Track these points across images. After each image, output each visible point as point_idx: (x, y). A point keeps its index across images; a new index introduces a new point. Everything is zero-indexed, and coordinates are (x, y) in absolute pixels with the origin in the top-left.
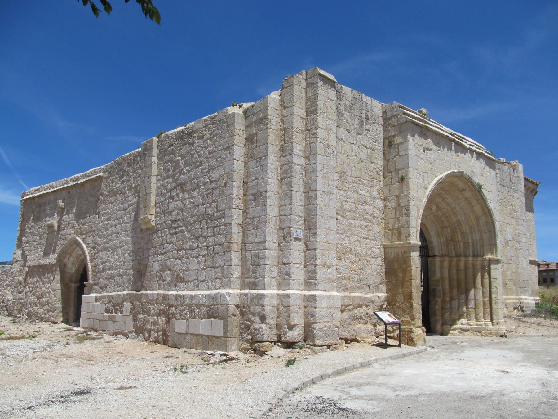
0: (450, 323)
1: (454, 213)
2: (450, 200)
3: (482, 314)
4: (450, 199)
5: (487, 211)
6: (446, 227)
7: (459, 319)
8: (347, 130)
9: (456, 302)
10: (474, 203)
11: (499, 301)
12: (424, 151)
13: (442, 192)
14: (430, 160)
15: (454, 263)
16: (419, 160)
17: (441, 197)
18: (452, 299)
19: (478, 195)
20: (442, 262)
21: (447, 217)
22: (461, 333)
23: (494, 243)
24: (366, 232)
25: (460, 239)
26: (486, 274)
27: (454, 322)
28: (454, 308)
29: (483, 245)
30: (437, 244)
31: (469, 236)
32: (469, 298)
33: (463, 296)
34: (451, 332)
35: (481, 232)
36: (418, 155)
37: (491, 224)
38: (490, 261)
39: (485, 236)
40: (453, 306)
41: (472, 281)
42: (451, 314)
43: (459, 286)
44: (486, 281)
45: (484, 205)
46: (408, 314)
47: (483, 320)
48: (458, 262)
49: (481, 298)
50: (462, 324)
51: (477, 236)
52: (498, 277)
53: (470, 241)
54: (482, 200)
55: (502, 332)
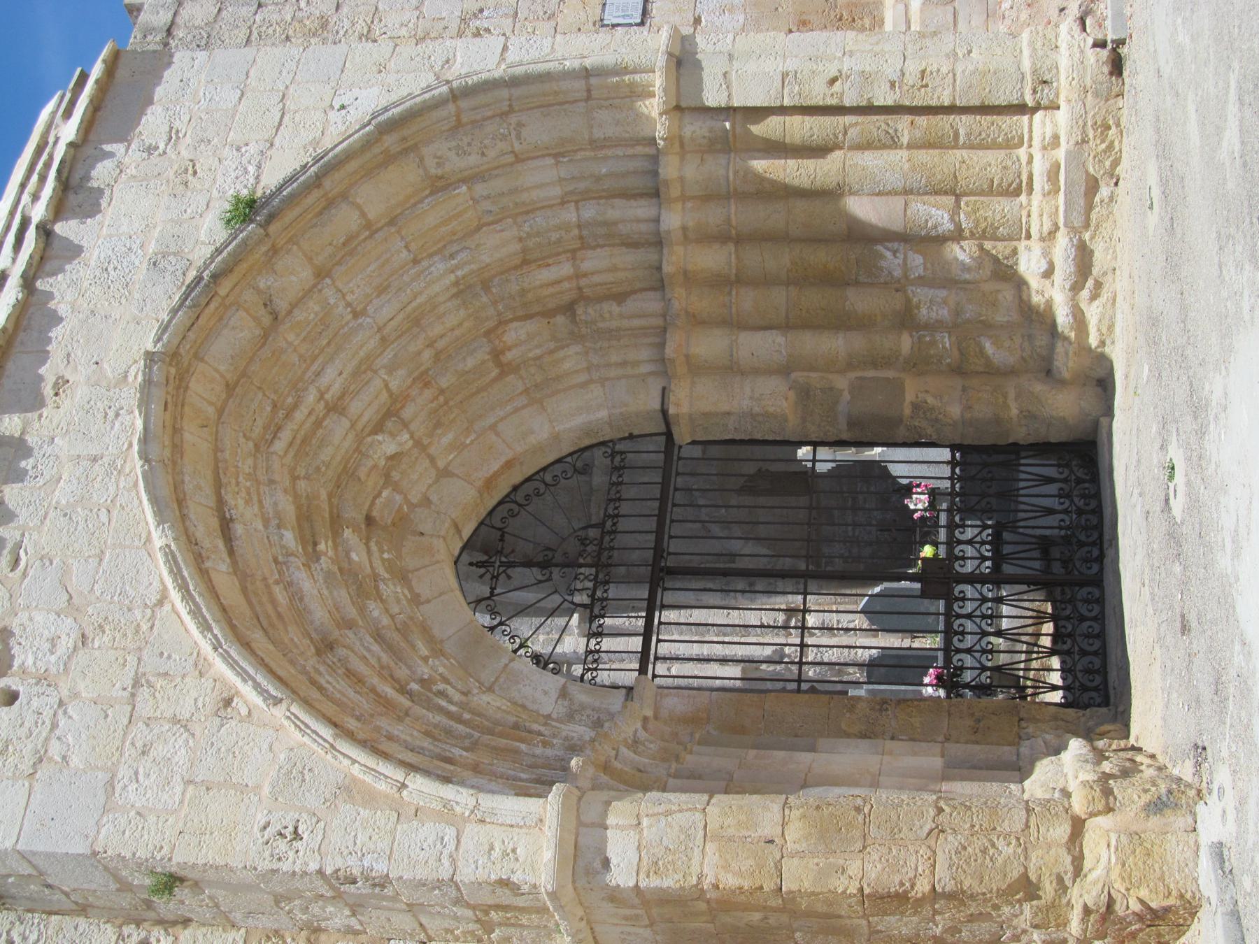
0: (1042, 340)
1: (416, 321)
2: (333, 378)
3: (992, 157)
4: (330, 373)
5: (390, 141)
6: (496, 355)
7: (1020, 284)
9: (920, 294)
10: (346, 220)
11: (913, 68)
13: (279, 446)
14: (65, 644)
15: (703, 303)
16: (55, 749)
17: (318, 424)
18: (906, 319)
19: (290, 215)
20: (697, 369)
21: (437, 357)
22: (1098, 285)
23: (580, 85)
25: (566, 269)
26: (756, 129)
27: (1037, 320)
28: (957, 313)
29: (595, 144)
30: (596, 391)
31: (539, 220)
32: (897, 225)
33: (891, 260)
34: (1093, 341)
35: (519, 159)
36: (26, 767)
37: (464, 104)
38: (684, 107)
39: (538, 131)
40: (944, 313)
41: (800, 205)
42: (986, 326)
43: (831, 280)
44: (799, 128)
45: (353, 165)
46: (996, 907)
47: (1022, 152)
48: (689, 278)
49: (898, 157)
50: (1048, 273)
51: (542, 179)
52: (773, 67)
53: (569, 215)
54: (327, 183)
55: (1096, 60)
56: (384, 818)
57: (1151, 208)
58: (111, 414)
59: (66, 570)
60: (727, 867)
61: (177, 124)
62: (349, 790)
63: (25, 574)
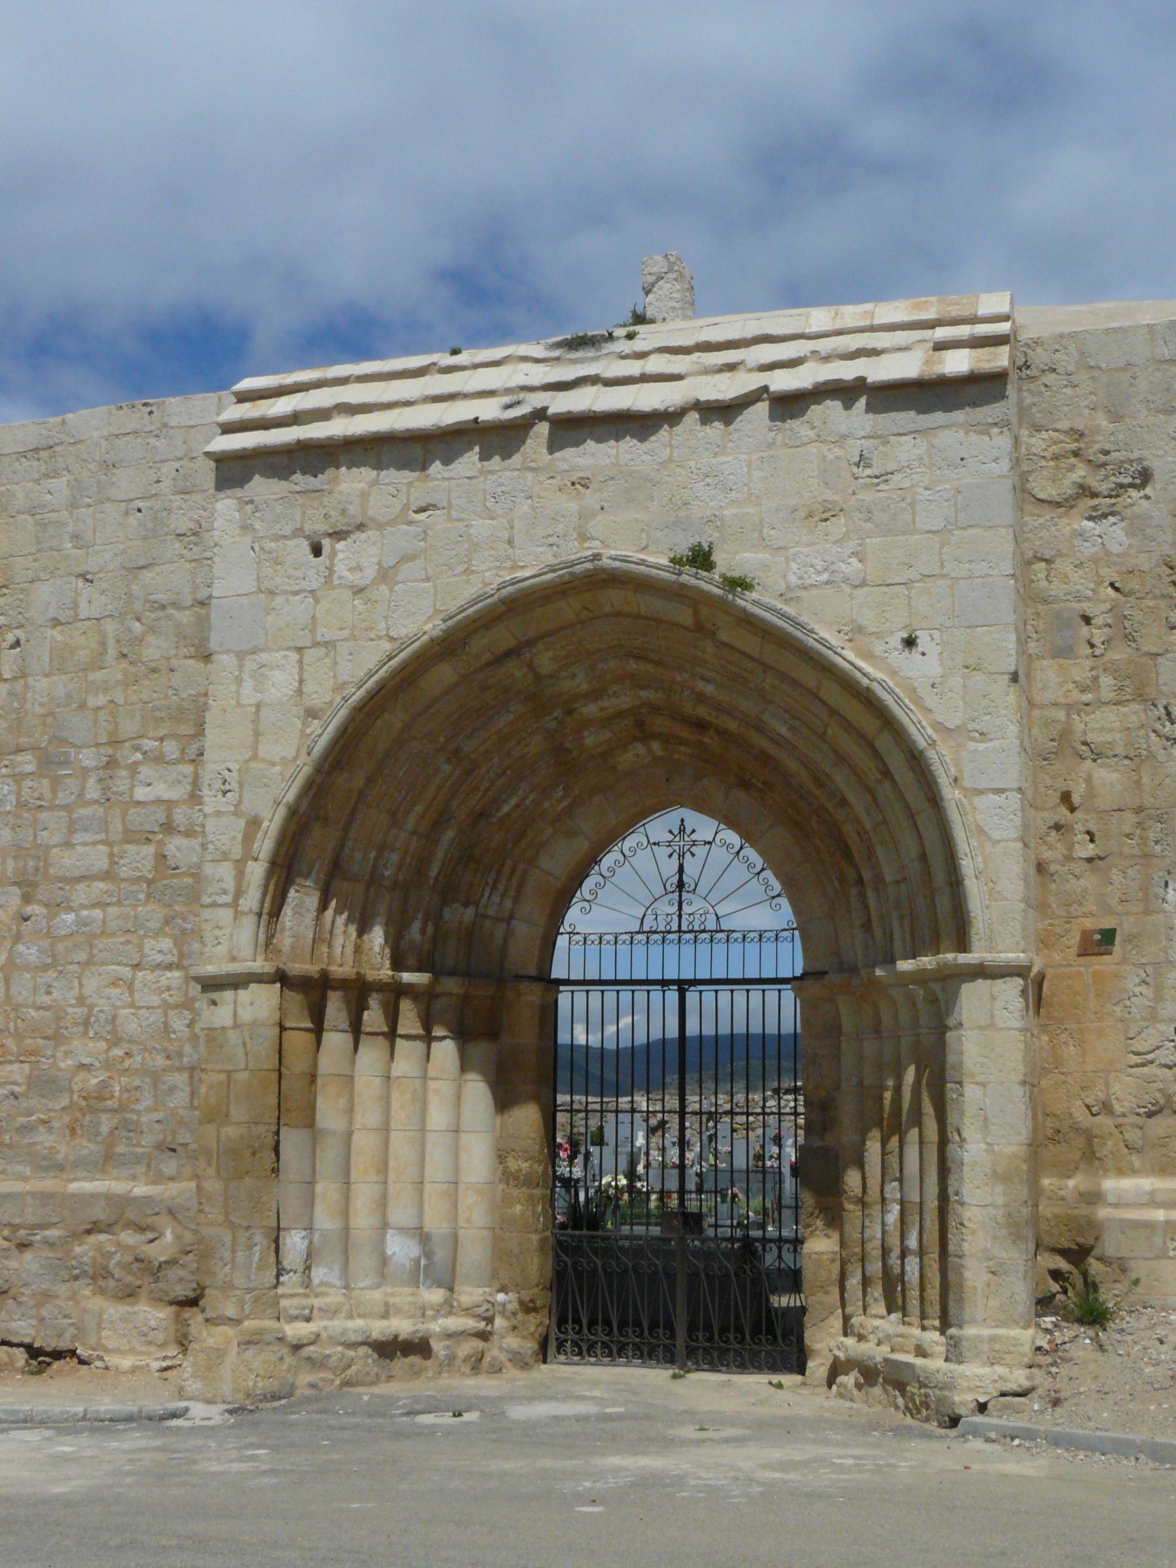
8: (83, 576)
12: (317, 551)
16: (279, 601)
24: (166, 943)
36: (266, 585)
56: (237, 851)
57: (702, 1429)
58: (551, 540)
59: (412, 558)
60: (211, 1087)
61: (897, 477)
62: (254, 823)
63: (410, 523)
